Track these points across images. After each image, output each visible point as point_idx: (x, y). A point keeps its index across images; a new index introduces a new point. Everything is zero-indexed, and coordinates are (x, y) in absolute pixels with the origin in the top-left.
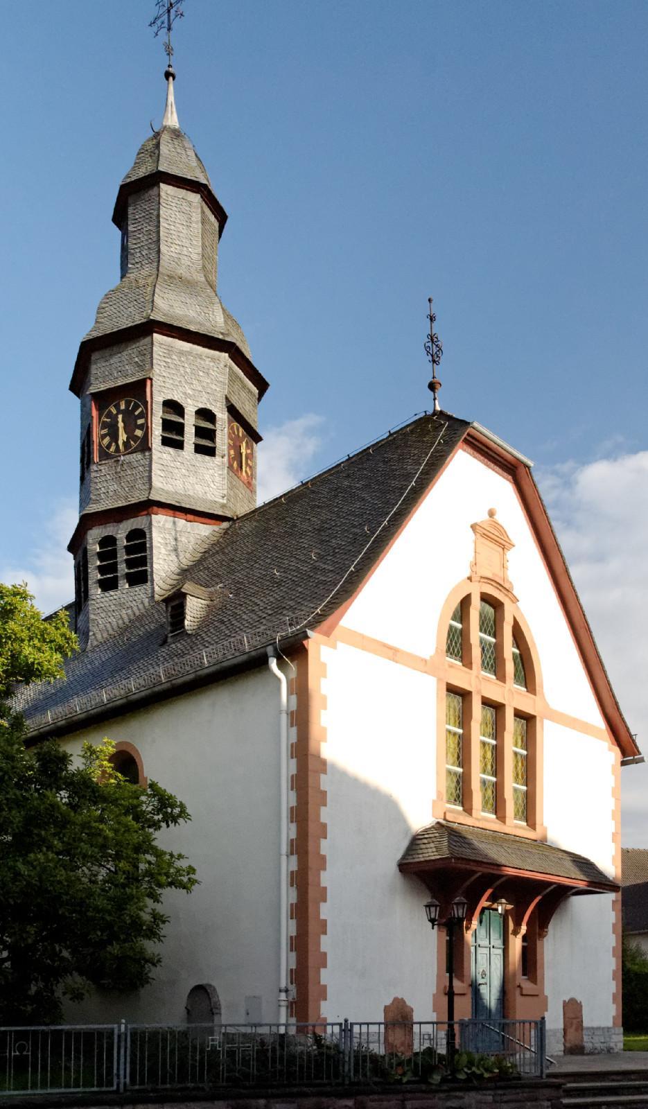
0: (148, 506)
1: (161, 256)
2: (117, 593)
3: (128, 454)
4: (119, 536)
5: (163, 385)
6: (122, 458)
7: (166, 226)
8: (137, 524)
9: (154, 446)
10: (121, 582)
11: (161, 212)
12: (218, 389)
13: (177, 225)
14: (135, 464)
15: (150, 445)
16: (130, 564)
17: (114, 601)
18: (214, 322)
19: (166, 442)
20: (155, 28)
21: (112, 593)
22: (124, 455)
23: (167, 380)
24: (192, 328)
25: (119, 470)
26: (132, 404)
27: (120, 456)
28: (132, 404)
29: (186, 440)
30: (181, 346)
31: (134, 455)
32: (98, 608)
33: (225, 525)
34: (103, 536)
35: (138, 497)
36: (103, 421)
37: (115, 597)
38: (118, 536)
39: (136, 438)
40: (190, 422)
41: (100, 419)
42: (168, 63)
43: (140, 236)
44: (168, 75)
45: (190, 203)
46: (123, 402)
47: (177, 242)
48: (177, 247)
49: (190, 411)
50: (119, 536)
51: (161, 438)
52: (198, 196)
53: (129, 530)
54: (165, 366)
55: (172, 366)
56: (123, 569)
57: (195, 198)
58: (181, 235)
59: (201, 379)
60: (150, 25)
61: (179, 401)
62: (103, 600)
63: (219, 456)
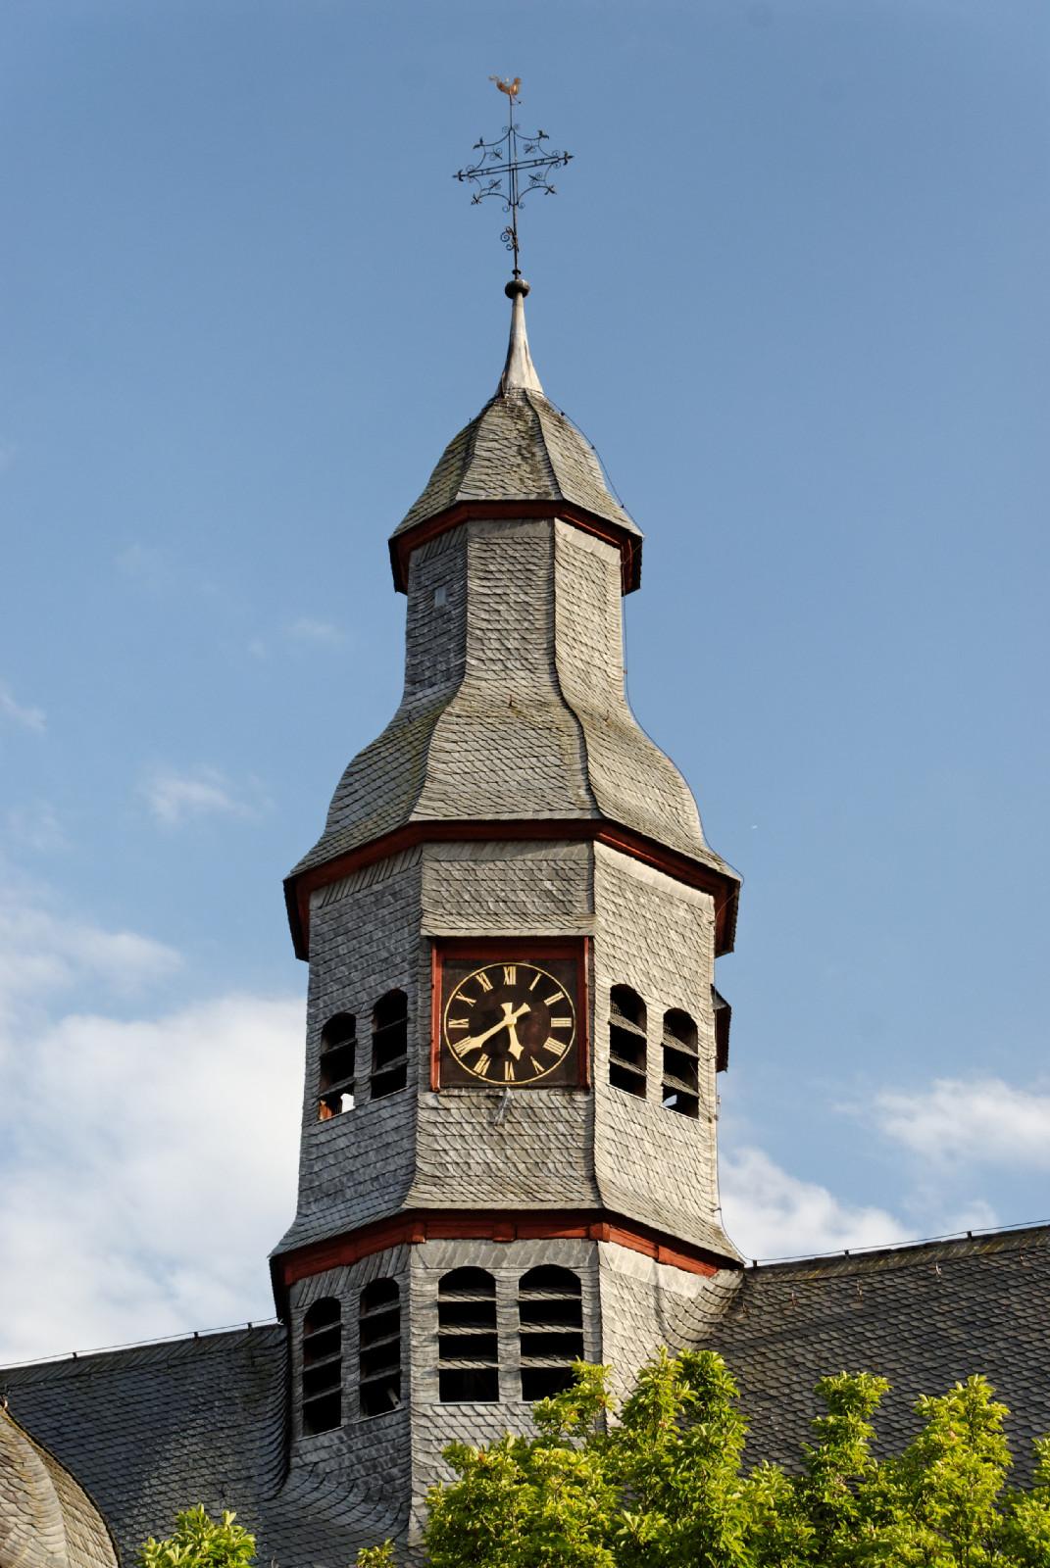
0: (595, 1221)
1: (558, 664)
2: (495, 1412)
3: (527, 1087)
4: (503, 1273)
5: (613, 952)
6: (509, 1093)
7: (565, 603)
8: (556, 1254)
9: (598, 1084)
10: (508, 1385)
11: (557, 575)
12: (700, 971)
13: (584, 605)
14: (547, 1116)
15: (589, 1081)
16: (531, 1345)
17: (487, 1430)
18: (687, 828)
19: (619, 1078)
20: (471, 188)
21: (481, 1409)
22: (513, 1087)
23: (618, 943)
24: (668, 841)
25: (499, 1119)
26: (538, 978)
27: (504, 1088)
28: (538, 978)
29: (649, 1078)
30: (640, 874)
31: (543, 1093)
32: (439, 1440)
33: (726, 1278)
34: (456, 1265)
35: (563, 1194)
36: (455, 1001)
37: (491, 1420)
38: (500, 1274)
39: (548, 1058)
40: (655, 1036)
41: (446, 993)
42: (514, 268)
43: (501, 608)
44: (514, 290)
45: (603, 564)
46: (513, 970)
47: (585, 640)
48: (583, 649)
49: (655, 1013)
50: (503, 1273)
51: (608, 1067)
52: (617, 552)
53: (531, 1265)
54: (613, 913)
55: (625, 913)
56: (510, 1355)
57: (612, 556)
58: (590, 626)
59: (673, 946)
60: (460, 177)
61: (637, 989)
62: (452, 1421)
63: (704, 1116)
